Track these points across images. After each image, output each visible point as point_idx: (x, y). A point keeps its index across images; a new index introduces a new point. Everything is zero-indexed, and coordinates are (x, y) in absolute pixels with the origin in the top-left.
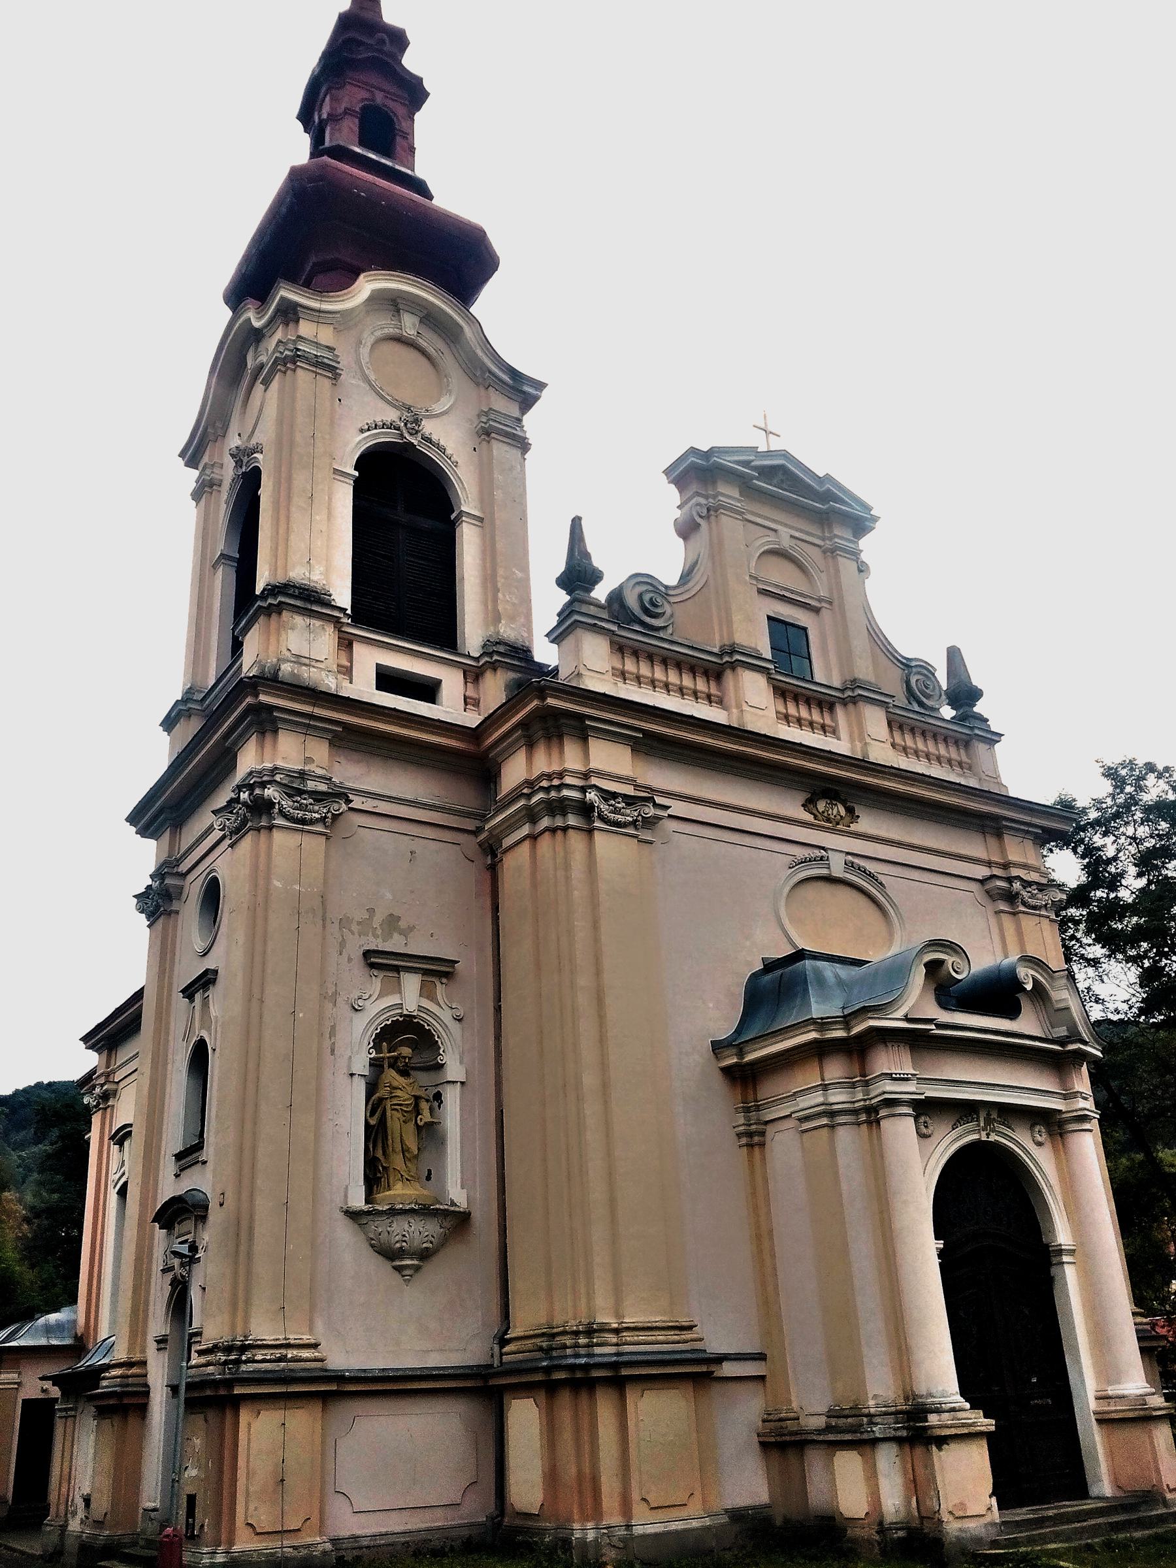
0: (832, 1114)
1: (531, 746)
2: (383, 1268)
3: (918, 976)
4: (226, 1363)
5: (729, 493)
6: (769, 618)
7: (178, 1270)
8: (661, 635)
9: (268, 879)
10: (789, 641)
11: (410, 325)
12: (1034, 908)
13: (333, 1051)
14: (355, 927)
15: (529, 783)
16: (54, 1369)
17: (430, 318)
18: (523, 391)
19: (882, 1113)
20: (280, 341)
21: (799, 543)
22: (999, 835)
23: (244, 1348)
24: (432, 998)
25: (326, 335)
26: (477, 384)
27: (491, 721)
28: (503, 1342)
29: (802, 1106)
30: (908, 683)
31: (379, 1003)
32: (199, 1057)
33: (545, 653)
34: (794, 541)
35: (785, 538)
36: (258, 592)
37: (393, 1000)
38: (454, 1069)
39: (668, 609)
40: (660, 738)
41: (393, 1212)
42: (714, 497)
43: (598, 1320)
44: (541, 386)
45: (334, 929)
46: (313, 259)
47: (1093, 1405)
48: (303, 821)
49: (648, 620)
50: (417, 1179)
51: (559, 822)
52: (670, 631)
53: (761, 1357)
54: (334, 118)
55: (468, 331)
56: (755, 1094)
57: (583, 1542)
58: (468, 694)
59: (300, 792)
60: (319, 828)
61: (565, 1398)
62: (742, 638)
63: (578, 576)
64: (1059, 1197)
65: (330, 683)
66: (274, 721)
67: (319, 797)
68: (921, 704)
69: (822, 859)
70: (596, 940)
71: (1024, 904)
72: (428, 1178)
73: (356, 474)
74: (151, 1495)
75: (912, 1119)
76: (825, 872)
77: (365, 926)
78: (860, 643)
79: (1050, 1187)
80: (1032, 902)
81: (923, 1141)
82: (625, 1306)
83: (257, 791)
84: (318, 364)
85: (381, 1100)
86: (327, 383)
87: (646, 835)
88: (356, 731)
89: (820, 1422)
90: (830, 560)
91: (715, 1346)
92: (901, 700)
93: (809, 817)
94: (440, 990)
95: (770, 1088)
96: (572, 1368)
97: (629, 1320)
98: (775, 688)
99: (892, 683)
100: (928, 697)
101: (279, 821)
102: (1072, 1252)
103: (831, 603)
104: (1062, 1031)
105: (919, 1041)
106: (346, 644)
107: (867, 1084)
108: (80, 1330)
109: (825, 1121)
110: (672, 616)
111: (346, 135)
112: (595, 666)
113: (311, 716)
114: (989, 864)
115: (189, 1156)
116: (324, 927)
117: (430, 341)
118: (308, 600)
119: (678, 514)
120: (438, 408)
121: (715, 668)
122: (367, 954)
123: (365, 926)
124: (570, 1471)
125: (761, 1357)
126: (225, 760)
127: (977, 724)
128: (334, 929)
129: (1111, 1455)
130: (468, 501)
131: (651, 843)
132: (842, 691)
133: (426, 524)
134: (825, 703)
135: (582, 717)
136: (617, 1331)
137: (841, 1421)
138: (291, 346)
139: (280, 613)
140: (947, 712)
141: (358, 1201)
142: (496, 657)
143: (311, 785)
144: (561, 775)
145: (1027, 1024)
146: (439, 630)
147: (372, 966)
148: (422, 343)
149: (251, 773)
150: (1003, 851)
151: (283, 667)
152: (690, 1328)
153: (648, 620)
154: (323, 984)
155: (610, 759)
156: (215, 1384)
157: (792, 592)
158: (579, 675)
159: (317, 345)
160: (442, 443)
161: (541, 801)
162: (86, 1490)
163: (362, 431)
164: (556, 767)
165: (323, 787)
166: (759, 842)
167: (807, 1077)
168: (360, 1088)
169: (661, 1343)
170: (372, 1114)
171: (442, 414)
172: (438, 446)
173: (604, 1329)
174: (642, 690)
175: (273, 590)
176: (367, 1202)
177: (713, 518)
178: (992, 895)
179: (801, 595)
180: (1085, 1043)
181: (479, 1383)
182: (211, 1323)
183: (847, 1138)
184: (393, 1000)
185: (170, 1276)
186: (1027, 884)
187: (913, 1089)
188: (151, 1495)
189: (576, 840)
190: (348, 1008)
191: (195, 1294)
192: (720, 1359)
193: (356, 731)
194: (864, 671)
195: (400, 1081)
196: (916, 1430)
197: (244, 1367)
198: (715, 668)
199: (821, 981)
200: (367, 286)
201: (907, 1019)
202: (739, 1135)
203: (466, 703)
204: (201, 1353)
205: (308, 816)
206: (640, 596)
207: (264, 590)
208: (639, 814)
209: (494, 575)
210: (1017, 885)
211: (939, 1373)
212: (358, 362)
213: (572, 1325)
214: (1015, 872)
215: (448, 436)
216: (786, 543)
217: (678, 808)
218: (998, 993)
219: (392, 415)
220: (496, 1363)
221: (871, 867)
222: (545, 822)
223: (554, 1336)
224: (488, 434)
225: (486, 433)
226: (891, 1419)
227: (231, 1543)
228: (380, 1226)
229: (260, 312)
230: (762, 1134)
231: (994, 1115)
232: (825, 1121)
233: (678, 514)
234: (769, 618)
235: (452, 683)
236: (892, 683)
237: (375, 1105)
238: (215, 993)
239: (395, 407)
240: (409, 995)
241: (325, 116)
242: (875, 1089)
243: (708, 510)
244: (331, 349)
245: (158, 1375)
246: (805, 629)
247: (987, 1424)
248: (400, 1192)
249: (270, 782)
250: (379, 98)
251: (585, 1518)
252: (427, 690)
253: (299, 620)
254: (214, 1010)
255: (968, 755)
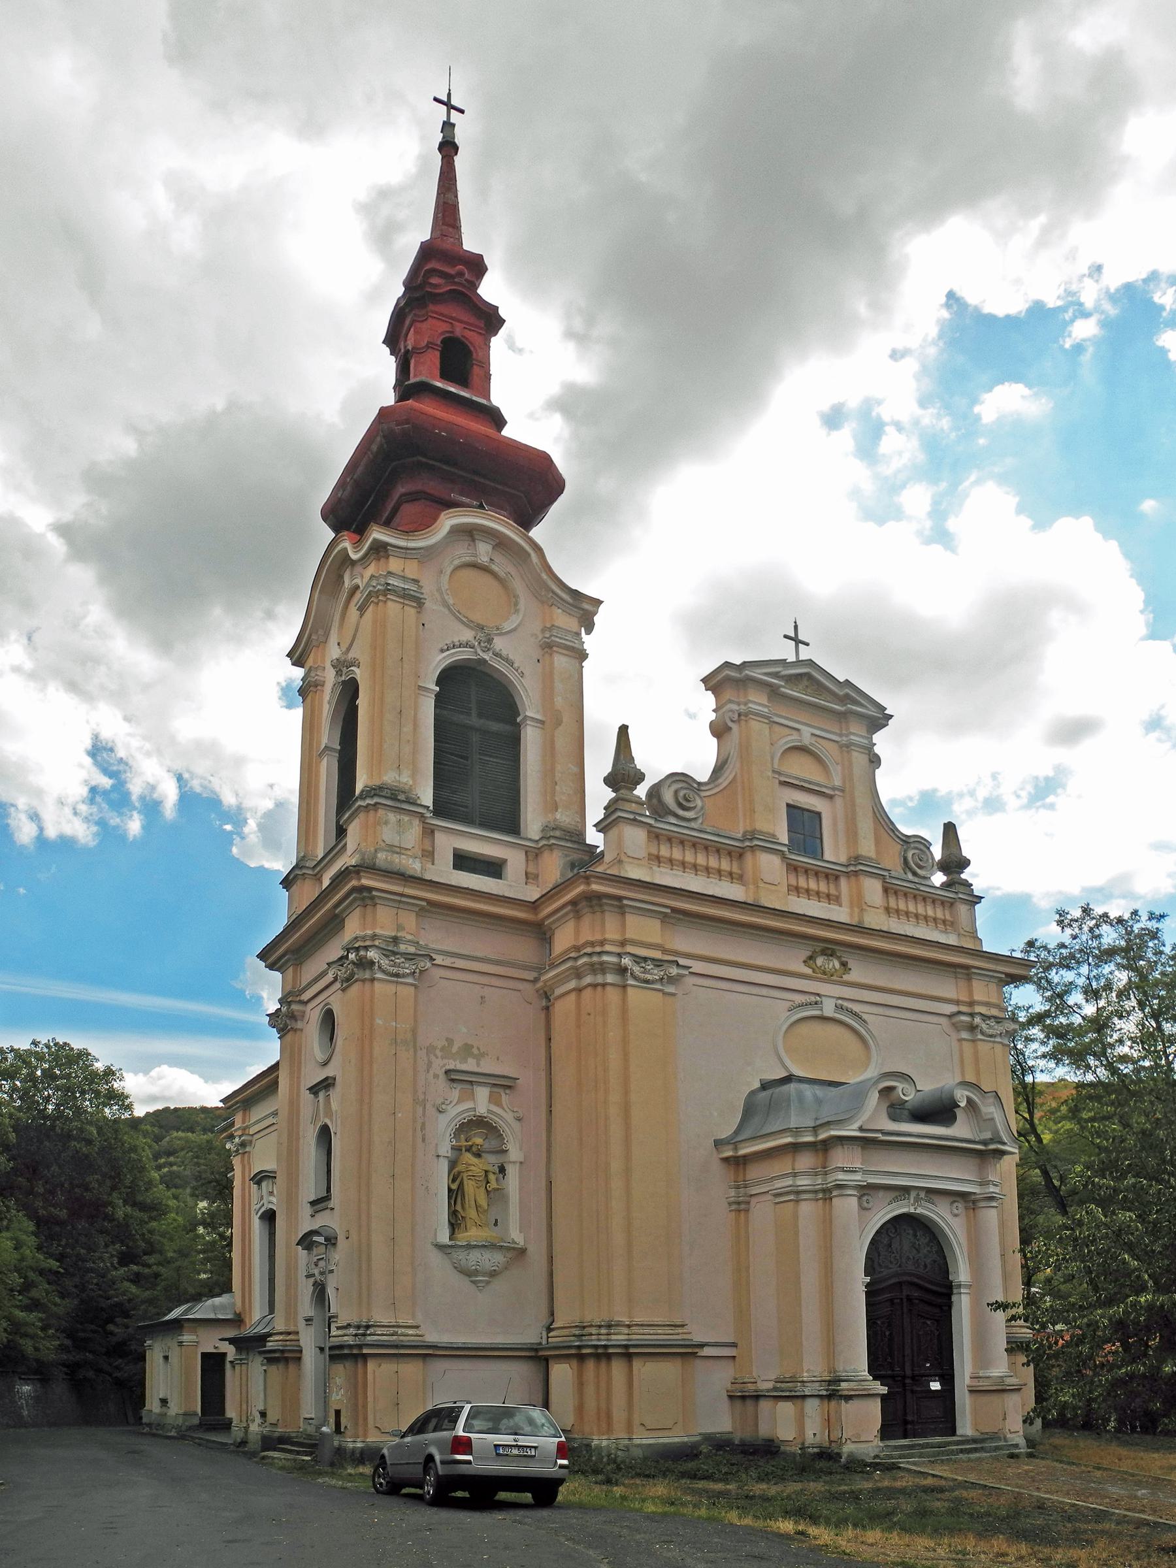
0: (798, 1193)
1: (578, 916)
2: (463, 1283)
3: (874, 1097)
4: (356, 1335)
5: (758, 700)
6: (788, 805)
7: (318, 1277)
8: (693, 825)
9: (372, 1019)
10: (805, 826)
11: (484, 551)
12: (991, 1036)
13: (424, 1140)
14: (439, 1053)
15: (577, 948)
16: (231, 1333)
17: (501, 543)
18: (584, 609)
19: (835, 1193)
20: (372, 576)
21: (819, 740)
22: (969, 978)
23: (368, 1327)
24: (500, 1105)
25: (412, 569)
26: (543, 602)
27: (546, 897)
28: (549, 1329)
29: (777, 1186)
30: (905, 859)
31: (457, 1111)
32: (325, 1134)
33: (594, 837)
34: (815, 738)
35: (806, 736)
36: (357, 792)
37: (468, 1105)
38: (515, 1153)
39: (699, 803)
40: (685, 911)
41: (469, 1247)
42: (746, 704)
43: (616, 1319)
44: (598, 602)
45: (422, 1054)
46: (400, 490)
47: (967, 1381)
48: (397, 975)
49: (681, 812)
50: (487, 1225)
51: (599, 979)
52: (700, 821)
53: (734, 1345)
54: (417, 351)
55: (534, 557)
56: (744, 1175)
57: (599, 1448)
58: (529, 870)
59: (395, 953)
60: (410, 980)
61: (590, 1365)
62: (762, 825)
63: (623, 775)
64: (965, 1249)
65: (415, 866)
66: (373, 898)
67: (410, 957)
68: (915, 874)
69: (816, 1003)
70: (626, 1068)
71: (982, 1033)
72: (496, 1224)
73: (438, 689)
74: (309, 1408)
75: (856, 1199)
76: (817, 1013)
77: (446, 1051)
78: (866, 826)
79: (959, 1244)
80: (991, 1032)
81: (863, 1212)
82: (636, 1312)
83: (362, 953)
84: (405, 595)
85: (459, 1173)
86: (413, 611)
87: (671, 989)
88: (441, 906)
89: (770, 1385)
90: (845, 754)
91: (698, 1338)
92: (898, 871)
93: (809, 971)
94: (505, 1099)
95: (755, 1172)
96: (596, 1347)
97: (637, 1320)
98: (788, 865)
99: (892, 861)
100: (920, 867)
101: (379, 975)
102: (966, 1286)
103: (843, 791)
104: (988, 1135)
105: (867, 1143)
106: (429, 832)
107: (826, 1174)
108: (238, 1309)
109: (792, 1197)
110: (702, 808)
111: (427, 371)
112: (634, 855)
113: (402, 895)
114: (957, 1002)
115: (320, 1203)
116: (415, 1052)
117: (502, 566)
118: (396, 798)
119: (713, 716)
120: (507, 626)
121: (737, 851)
122: (447, 1072)
123: (446, 1051)
124: (591, 1404)
125: (734, 1345)
126: (334, 923)
127: (961, 889)
128: (422, 1054)
129: (975, 1412)
130: (530, 707)
131: (673, 995)
132: (847, 866)
133: (495, 726)
134: (832, 876)
135: (620, 898)
136: (629, 1326)
137: (783, 1385)
138: (382, 581)
139: (376, 811)
140: (939, 878)
141: (444, 1238)
142: (553, 841)
143: (403, 948)
144: (602, 943)
145: (961, 1129)
146: (507, 821)
147: (453, 1080)
148: (494, 567)
149: (356, 938)
150: (971, 992)
151: (379, 855)
152: (683, 1326)
153: (681, 812)
154: (415, 1092)
155: (644, 930)
156: (351, 1347)
157: (810, 783)
158: (620, 862)
159: (404, 578)
160: (511, 657)
161: (585, 964)
162: (261, 1408)
163: (442, 651)
164: (598, 937)
165: (412, 950)
166: (764, 991)
167: (781, 1166)
168: (444, 1166)
169: (662, 1335)
170: (454, 1181)
171: (514, 630)
172: (507, 660)
173: (619, 1324)
174: (674, 872)
175: (370, 792)
176: (451, 1239)
177: (743, 723)
178: (957, 1027)
179: (818, 785)
180: (1004, 1144)
181: (533, 1354)
182: (343, 1310)
183: (808, 1209)
184: (468, 1105)
185: (312, 1280)
186: (985, 1017)
187: (859, 1178)
188: (309, 1408)
189: (613, 995)
190: (434, 1110)
191: (330, 1291)
192: (702, 1346)
193: (441, 906)
194: (867, 848)
195: (475, 1160)
196: (833, 1392)
197: (369, 1338)
198: (737, 851)
199: (801, 1099)
200: (448, 521)
201: (861, 1129)
202: (730, 1204)
203: (527, 878)
204: (338, 1328)
205: (401, 971)
206: (676, 792)
207: (362, 791)
208: (666, 971)
209: (553, 769)
210: (977, 1020)
211: (856, 1359)
212: (439, 590)
213: (597, 1322)
214: (978, 1009)
215: (516, 654)
216: (806, 739)
217: (698, 967)
218: (940, 1111)
219: (467, 635)
220: (544, 1342)
221: (856, 1008)
222: (588, 979)
223: (584, 1327)
224: (550, 647)
225: (548, 647)
226: (817, 1384)
227: (365, 1436)
228: (461, 1255)
229: (357, 544)
230: (748, 1203)
231: (922, 1195)
232: (792, 1197)
233: (713, 716)
234: (788, 805)
235: (515, 861)
236: (892, 861)
237: (455, 1177)
238: (335, 1094)
239: (472, 629)
240: (482, 1102)
241: (410, 347)
242: (831, 1178)
243: (739, 715)
244: (416, 581)
245: (308, 1341)
246: (819, 814)
247: (884, 1390)
248: (472, 1234)
249: (371, 946)
250: (459, 331)
251: (600, 1433)
252: (493, 868)
253: (392, 817)
254: (334, 1106)
255: (951, 914)
